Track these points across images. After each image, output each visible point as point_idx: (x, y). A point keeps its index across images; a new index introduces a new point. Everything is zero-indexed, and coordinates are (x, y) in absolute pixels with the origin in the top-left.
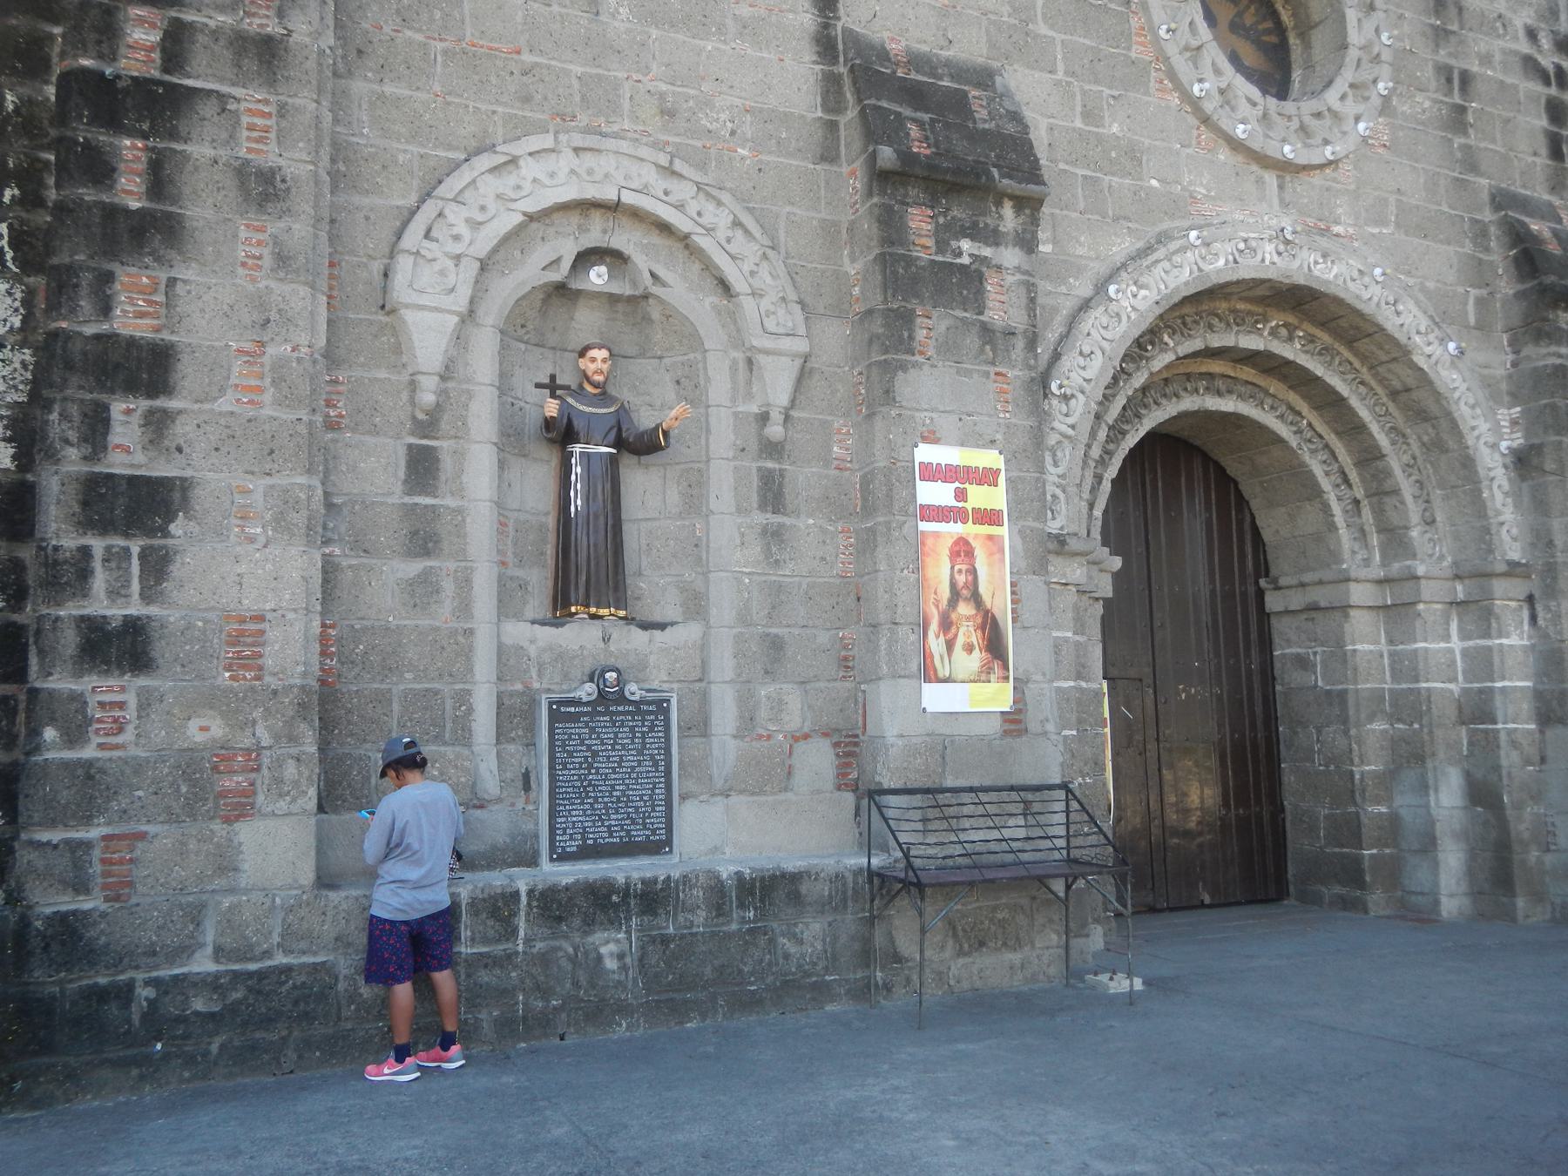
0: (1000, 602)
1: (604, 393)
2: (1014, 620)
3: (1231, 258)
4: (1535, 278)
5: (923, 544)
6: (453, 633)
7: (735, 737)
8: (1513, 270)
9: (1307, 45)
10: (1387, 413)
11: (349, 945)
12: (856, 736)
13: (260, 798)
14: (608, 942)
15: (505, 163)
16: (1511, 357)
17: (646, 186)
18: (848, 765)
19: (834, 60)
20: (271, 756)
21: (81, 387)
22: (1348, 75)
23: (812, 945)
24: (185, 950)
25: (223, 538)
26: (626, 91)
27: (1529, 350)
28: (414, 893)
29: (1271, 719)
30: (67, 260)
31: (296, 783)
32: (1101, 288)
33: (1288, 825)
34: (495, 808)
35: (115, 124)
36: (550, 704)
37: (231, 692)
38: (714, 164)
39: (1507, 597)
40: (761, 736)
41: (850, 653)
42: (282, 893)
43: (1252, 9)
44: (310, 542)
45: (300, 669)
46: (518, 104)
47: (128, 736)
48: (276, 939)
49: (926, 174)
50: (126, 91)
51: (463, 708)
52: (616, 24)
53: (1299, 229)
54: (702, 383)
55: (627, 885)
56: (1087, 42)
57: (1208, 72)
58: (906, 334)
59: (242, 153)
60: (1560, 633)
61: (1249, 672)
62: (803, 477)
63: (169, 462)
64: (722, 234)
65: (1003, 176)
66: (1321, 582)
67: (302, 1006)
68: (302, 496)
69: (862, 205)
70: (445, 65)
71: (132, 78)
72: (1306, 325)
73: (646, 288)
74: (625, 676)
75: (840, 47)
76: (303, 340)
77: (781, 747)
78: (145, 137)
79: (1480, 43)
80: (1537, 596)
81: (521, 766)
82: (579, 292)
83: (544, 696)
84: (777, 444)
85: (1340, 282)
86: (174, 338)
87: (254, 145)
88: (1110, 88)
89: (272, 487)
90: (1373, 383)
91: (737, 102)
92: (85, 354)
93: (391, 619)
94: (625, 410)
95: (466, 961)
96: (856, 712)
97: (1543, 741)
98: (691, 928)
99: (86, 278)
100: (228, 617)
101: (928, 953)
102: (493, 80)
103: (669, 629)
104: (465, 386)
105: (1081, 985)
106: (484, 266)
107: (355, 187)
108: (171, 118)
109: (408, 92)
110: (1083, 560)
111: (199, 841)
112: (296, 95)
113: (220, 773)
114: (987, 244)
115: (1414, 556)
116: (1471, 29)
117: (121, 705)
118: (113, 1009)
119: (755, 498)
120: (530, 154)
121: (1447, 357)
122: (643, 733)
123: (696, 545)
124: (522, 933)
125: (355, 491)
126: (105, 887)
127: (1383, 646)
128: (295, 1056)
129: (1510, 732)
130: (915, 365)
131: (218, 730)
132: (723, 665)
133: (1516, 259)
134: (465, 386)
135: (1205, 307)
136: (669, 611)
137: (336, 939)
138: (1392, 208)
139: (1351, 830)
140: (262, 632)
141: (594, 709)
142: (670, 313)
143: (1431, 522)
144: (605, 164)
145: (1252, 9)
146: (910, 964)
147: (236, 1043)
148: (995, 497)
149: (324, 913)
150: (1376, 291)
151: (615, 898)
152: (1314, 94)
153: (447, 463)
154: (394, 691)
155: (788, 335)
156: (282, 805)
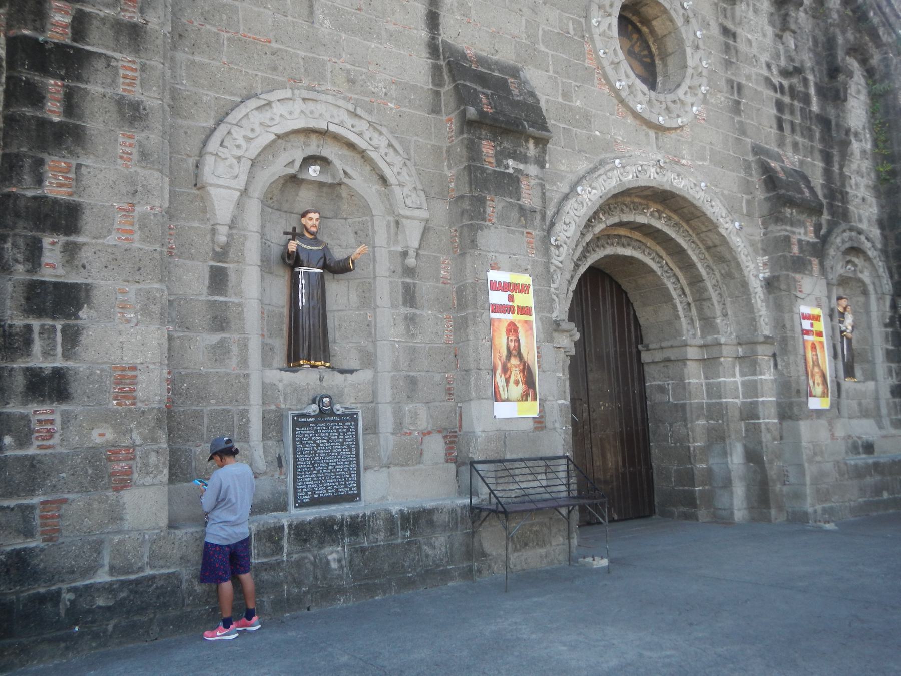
0: (530, 354)
1: (316, 239)
2: (539, 367)
3: (635, 175)
4: (775, 191)
5: (493, 325)
6: (238, 376)
7: (392, 434)
8: (763, 186)
9: (665, 65)
10: (705, 258)
11: (188, 561)
12: (456, 432)
13: (135, 476)
14: (332, 553)
15: (265, 105)
16: (763, 231)
17: (342, 122)
18: (452, 448)
19: (438, 57)
20: (141, 451)
21: (25, 228)
22: (687, 83)
23: (440, 549)
24: (91, 570)
25: (111, 320)
26: (329, 67)
27: (772, 227)
28: (232, 528)
29: (645, 420)
30: (16, 151)
31: (157, 466)
32: (573, 188)
33: (655, 475)
34: (263, 478)
35: (44, 70)
36: (293, 417)
37: (117, 412)
38: (376, 111)
39: (764, 354)
40: (406, 433)
41: (452, 386)
42: (149, 532)
43: (638, 44)
44: (162, 324)
45: (158, 398)
46: (269, 71)
47: (56, 440)
48: (146, 560)
49: (492, 123)
50: (50, 50)
51: (244, 420)
52: (323, 29)
53: (667, 161)
54: (371, 234)
55: (343, 519)
56: (564, 56)
57: (623, 77)
58: (482, 210)
59: (120, 91)
60: (789, 372)
61: (634, 394)
62: (426, 288)
63: (77, 274)
64: (383, 150)
65: (530, 126)
66: (672, 346)
67: (162, 599)
68: (158, 295)
69: (456, 138)
70: (229, 46)
71: (54, 43)
72: (667, 211)
73: (341, 179)
74: (334, 401)
75: (441, 50)
76: (157, 203)
77: (416, 439)
78: (62, 79)
79: (746, 69)
80: (778, 353)
81: (276, 453)
82: (303, 180)
83: (290, 412)
84: (412, 269)
85: (686, 189)
86: (81, 200)
87: (127, 87)
88: (575, 81)
89: (140, 290)
90: (698, 242)
91: (388, 77)
92: (27, 208)
94: (328, 249)
95: (255, 567)
96: (456, 419)
97: (781, 429)
98: (377, 542)
99: (28, 162)
100: (115, 367)
101: (504, 553)
102: (255, 56)
103: (355, 373)
104: (243, 233)
105: (577, 565)
106: (254, 163)
107: (178, 114)
108: (77, 69)
109: (207, 61)
110: (568, 334)
111: (99, 503)
112: (151, 59)
113: (111, 461)
114: (521, 163)
115: (718, 333)
116: (741, 62)
117: (51, 422)
118: (48, 607)
119: (401, 299)
120: (279, 100)
121: (735, 230)
122: (344, 432)
123: (368, 326)
124: (285, 550)
125: (181, 293)
126: (43, 533)
127: (703, 380)
128: (158, 630)
129: (766, 424)
130: (487, 227)
131: (110, 435)
132: (386, 393)
133: (765, 181)
134: (243, 233)
135: (619, 200)
136: (353, 364)
137: (181, 558)
138: (708, 152)
139: (689, 477)
140: (135, 376)
141: (317, 419)
142: (353, 194)
143: (725, 315)
144: (321, 108)
145: (638, 44)
146: (490, 557)
147: (123, 624)
148: (526, 300)
149: (173, 543)
150: (702, 195)
151: (336, 527)
152: (671, 91)
153: (232, 278)
154: (204, 410)
155: (418, 208)
156: (148, 480)
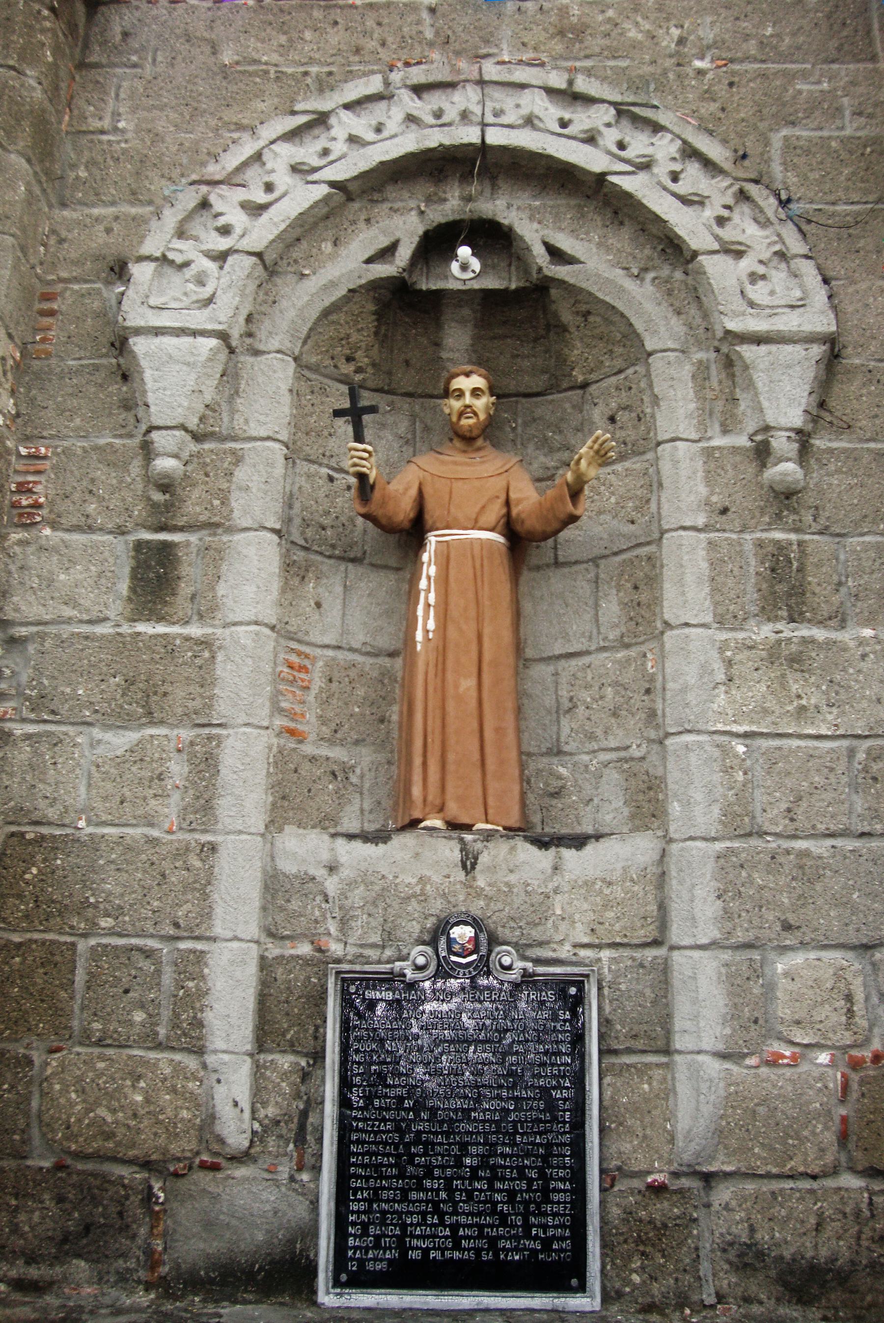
64: (662, 170)
82: (438, 295)
93: (82, 824)
103: (590, 848)
120: (347, 107)
123: (648, 691)
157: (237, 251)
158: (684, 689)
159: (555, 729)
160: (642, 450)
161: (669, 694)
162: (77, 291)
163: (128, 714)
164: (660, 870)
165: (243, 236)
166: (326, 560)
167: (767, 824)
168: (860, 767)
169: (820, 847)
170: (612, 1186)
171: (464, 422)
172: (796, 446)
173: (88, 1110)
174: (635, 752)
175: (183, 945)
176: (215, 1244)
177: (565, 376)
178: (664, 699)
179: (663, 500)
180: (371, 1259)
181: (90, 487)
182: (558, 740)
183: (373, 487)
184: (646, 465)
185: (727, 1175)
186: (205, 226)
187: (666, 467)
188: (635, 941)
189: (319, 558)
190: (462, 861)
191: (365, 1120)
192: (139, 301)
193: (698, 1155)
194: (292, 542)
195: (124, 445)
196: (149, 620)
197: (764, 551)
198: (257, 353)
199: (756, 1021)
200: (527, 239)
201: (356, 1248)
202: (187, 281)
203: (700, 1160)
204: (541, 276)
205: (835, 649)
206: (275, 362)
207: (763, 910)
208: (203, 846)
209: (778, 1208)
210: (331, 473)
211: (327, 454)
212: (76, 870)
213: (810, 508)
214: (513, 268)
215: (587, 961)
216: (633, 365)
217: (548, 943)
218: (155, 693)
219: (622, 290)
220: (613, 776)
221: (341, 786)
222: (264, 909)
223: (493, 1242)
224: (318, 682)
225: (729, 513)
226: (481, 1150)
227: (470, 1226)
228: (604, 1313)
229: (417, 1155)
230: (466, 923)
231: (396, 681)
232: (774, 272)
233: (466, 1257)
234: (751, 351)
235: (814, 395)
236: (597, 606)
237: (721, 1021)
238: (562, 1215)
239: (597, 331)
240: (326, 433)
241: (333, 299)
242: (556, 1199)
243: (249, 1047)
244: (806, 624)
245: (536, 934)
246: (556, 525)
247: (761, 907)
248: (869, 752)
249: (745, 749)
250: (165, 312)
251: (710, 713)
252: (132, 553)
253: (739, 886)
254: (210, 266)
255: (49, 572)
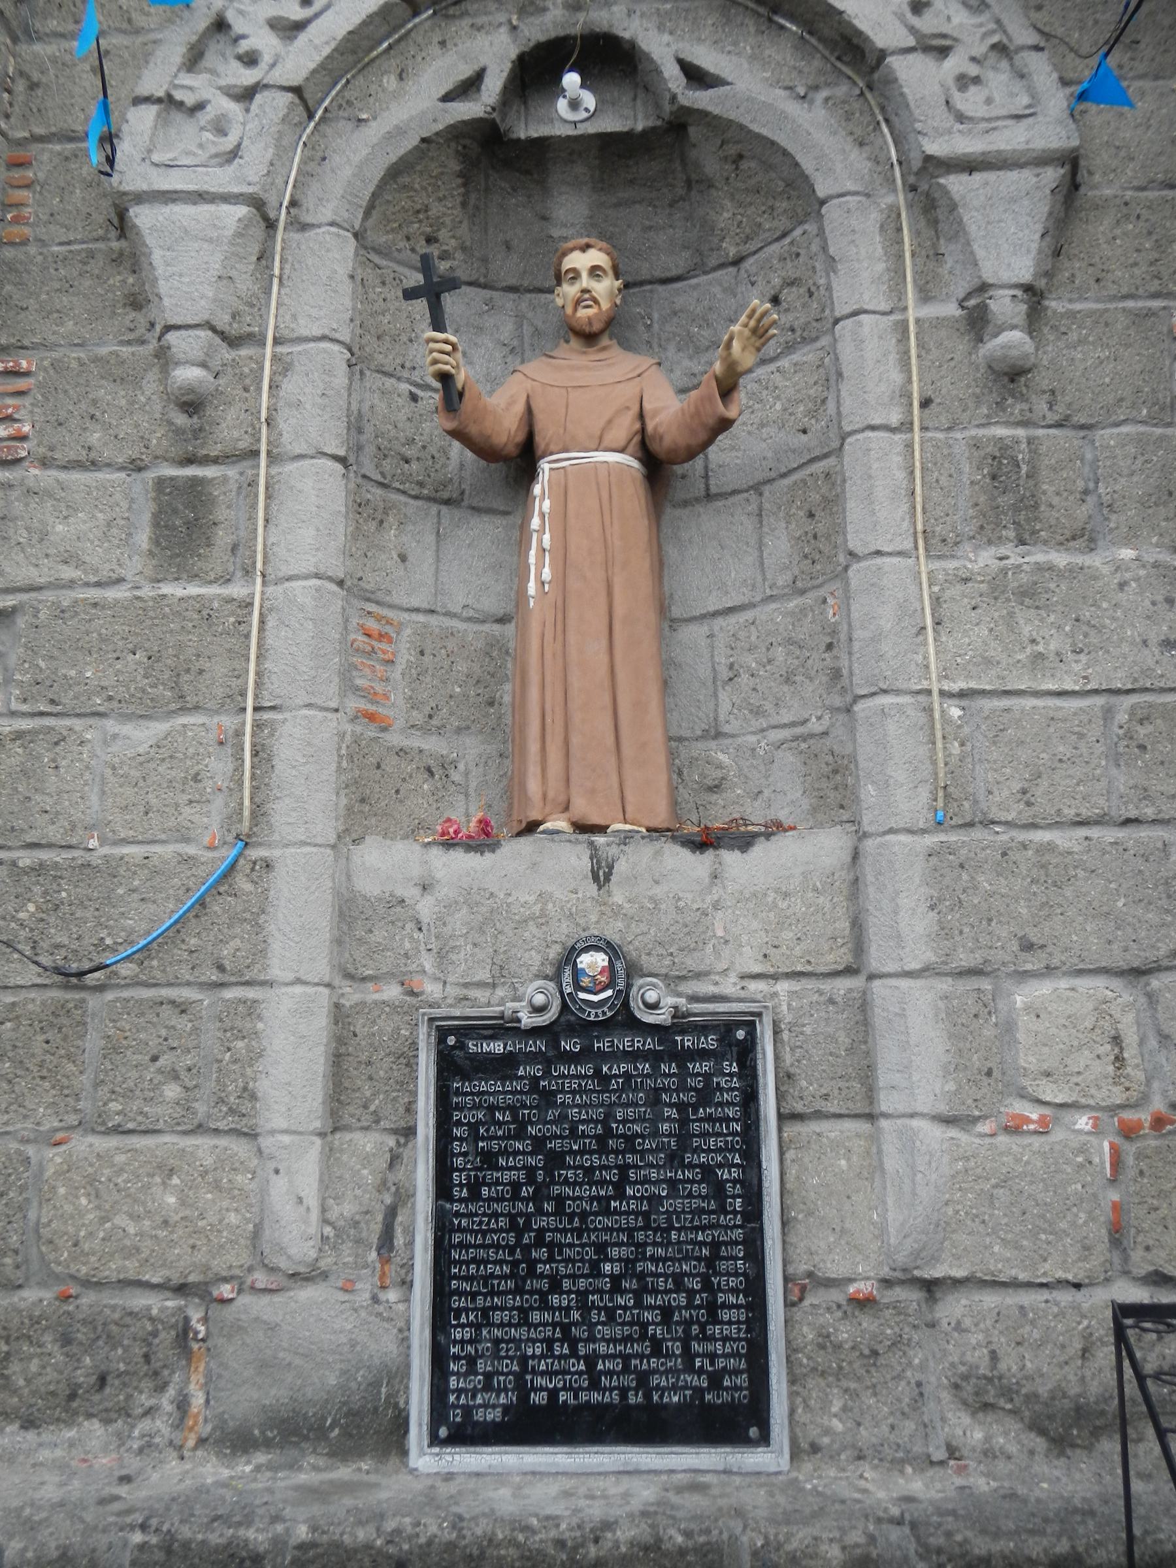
82: (541, 145)
93: (93, 843)
103: (759, 849)
157: (266, 86)
158: (876, 639)
159: (712, 705)
160: (814, 335)
161: (856, 646)
162: (59, 154)
163: (152, 700)
164: (851, 876)
165: (273, 65)
166: (412, 501)
167: (994, 809)
168: (1121, 732)
169: (1062, 839)
170: (801, 1299)
171: (582, 313)
172: (1024, 307)
173: (104, 1220)
174: (815, 726)
175: (229, 994)
176: (273, 1392)
177: (712, 250)
178: (850, 653)
179: (843, 393)
180: (480, 1406)
181: (92, 411)
182: (716, 719)
183: (461, 395)
184: (821, 354)
185: (957, 1283)
186: (223, 55)
187: (846, 351)
188: (822, 969)
189: (403, 498)
190: (592, 871)
191: (470, 1215)
192: (138, 157)
193: (916, 1254)
194: (364, 476)
195: (133, 354)
196: (177, 579)
197: (982, 453)
198: (304, 227)
199: (989, 1073)
200: (655, 56)
201: (459, 1391)
202: (202, 129)
203: (919, 1262)
204: (675, 108)
205: (1081, 577)
206: (328, 237)
207: (993, 924)
208: (255, 863)
209: (1028, 1328)
210: (414, 389)
211: (408, 365)
212: (87, 903)
213: (1044, 392)
214: (639, 102)
215: (759, 997)
216: (801, 223)
217: (707, 974)
218: (188, 671)
219: (784, 116)
220: (787, 759)
221: (439, 785)
222: (339, 942)
223: (643, 1379)
224: (405, 655)
225: (933, 406)
226: (625, 1252)
227: (613, 1357)
228: (794, 1474)
229: (540, 1261)
230: (597, 948)
231: (507, 653)
232: (991, 75)
233: (607, 1400)
234: (961, 183)
235: (1048, 239)
236: (760, 546)
237: (941, 1073)
238: (735, 1340)
239: (753, 181)
240: (404, 338)
241: (402, 152)
242: (726, 1318)
243: (318, 1124)
244: (1040, 546)
245: (691, 962)
246: (703, 436)
247: (990, 920)
248: (1132, 711)
249: (961, 713)
250: (174, 171)
251: (913, 667)
252: (153, 494)
253: (959, 892)
254: (233, 108)
255: (41, 521)
